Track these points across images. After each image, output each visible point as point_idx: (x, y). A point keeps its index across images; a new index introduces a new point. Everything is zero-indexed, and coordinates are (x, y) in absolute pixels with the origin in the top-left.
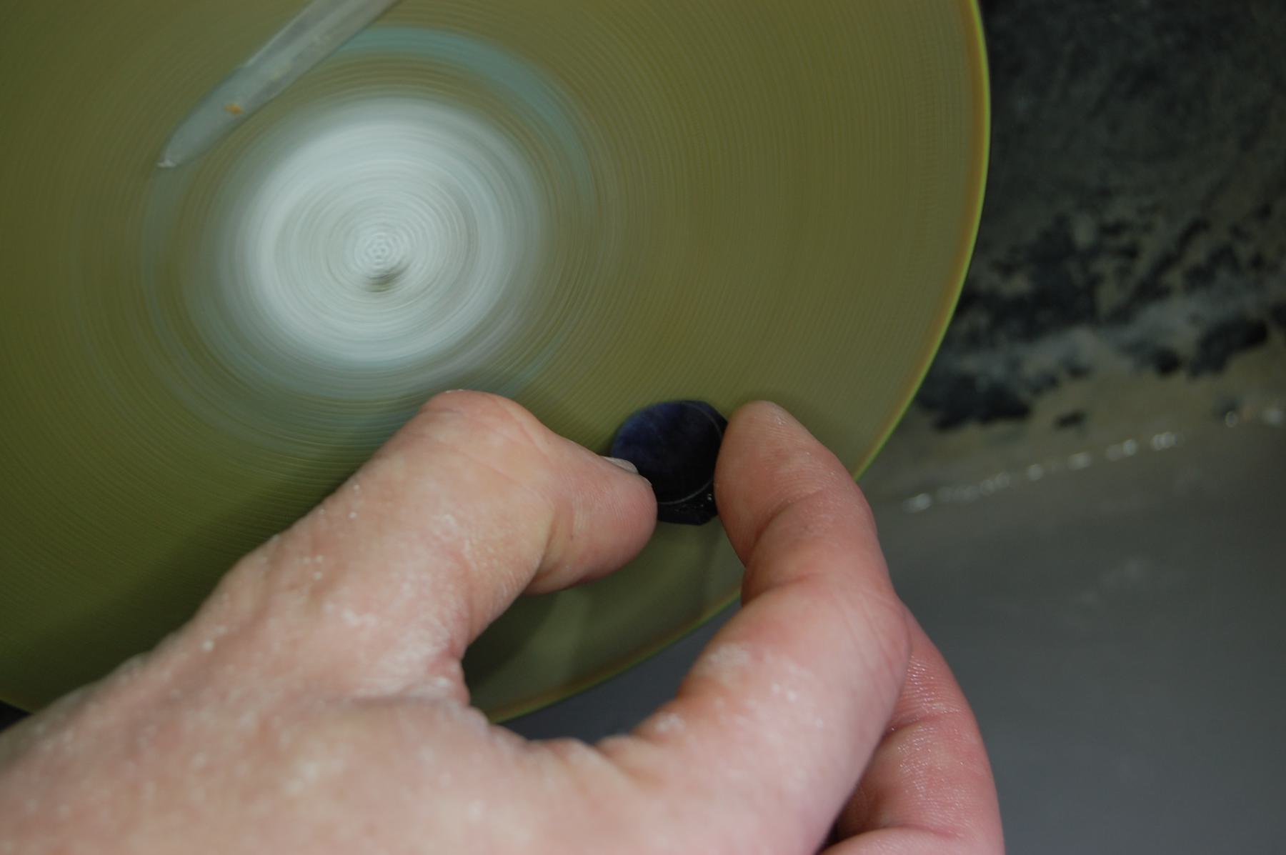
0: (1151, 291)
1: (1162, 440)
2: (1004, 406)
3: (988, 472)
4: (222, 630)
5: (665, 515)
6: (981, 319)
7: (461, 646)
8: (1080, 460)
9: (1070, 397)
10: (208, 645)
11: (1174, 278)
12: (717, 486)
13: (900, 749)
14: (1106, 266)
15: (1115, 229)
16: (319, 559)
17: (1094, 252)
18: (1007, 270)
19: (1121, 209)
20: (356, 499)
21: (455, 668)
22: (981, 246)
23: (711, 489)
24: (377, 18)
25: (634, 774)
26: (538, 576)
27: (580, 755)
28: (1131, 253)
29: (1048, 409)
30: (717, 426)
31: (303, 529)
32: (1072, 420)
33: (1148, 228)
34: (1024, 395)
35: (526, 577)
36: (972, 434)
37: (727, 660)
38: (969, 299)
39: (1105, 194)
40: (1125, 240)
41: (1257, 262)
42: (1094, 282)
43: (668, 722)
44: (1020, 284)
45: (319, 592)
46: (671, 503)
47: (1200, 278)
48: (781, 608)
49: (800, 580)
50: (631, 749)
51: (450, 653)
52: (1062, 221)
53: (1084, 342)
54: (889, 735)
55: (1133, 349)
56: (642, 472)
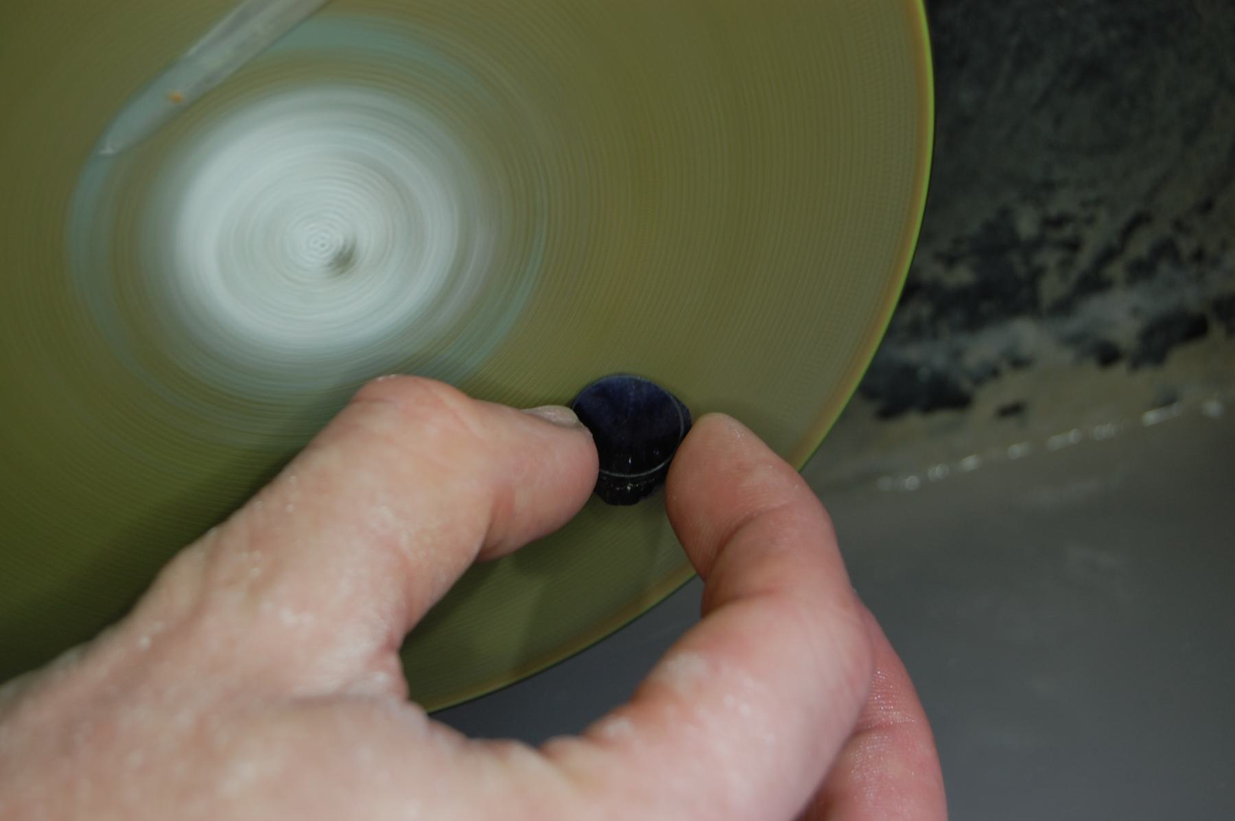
0: (1093, 284)
1: (1105, 430)
2: (946, 396)
3: (935, 462)
4: (158, 626)
6: (924, 310)
7: (398, 637)
8: (1017, 450)
9: (1011, 388)
10: (145, 642)
11: (1116, 270)
14: (1049, 258)
15: (1059, 222)
16: (257, 555)
17: (1037, 244)
18: (950, 261)
19: (1063, 202)
20: (293, 487)
21: (393, 661)
22: (926, 236)
24: (265, 471)
28: (1073, 246)
29: (989, 399)
30: (682, 427)
31: (241, 522)
32: (1013, 410)
33: (1090, 221)
34: (966, 385)
36: (914, 422)
37: (684, 669)
38: (912, 290)
39: (1049, 186)
40: (1068, 232)
41: (1199, 256)
42: (1036, 274)
43: (618, 727)
44: (963, 275)
45: (257, 590)
47: (1141, 270)
50: (577, 753)
51: (388, 647)
52: (1005, 213)
53: (1026, 334)
55: (1074, 341)
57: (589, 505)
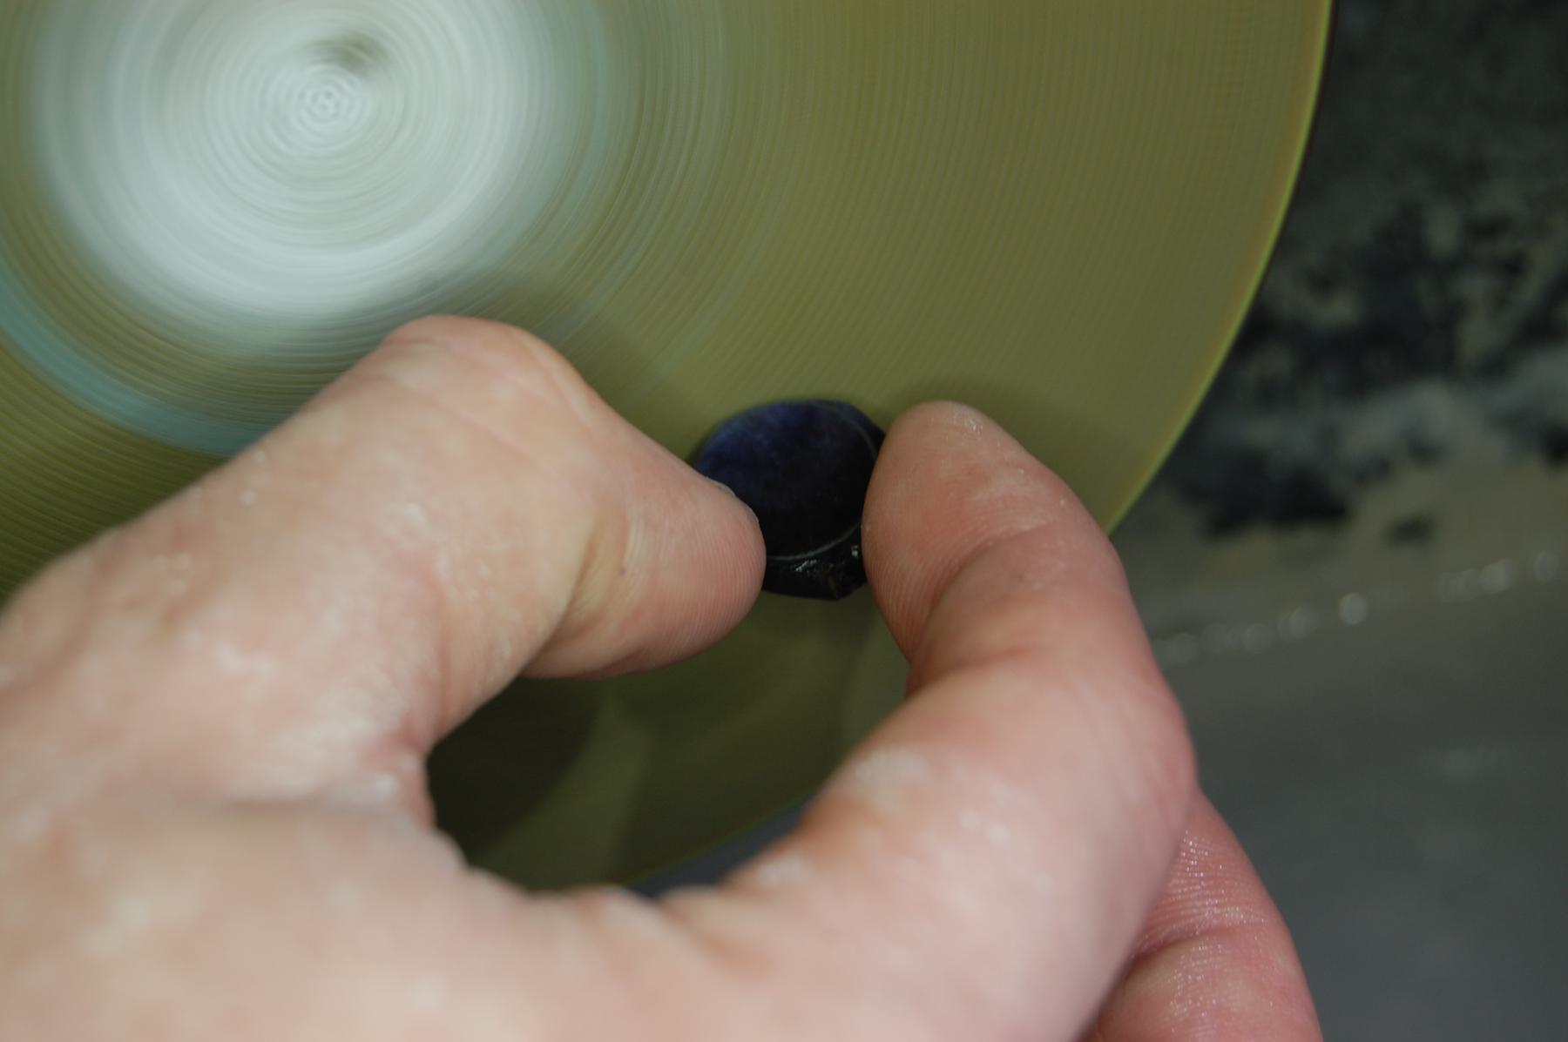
2: (1307, 502)
5: (776, 580)
6: (1276, 361)
7: (427, 735)
9: (1412, 492)
12: (867, 528)
13: (1166, 979)
14: (1475, 287)
15: (1491, 229)
16: (184, 561)
18: (1323, 284)
19: (1501, 198)
21: (411, 766)
22: (1286, 244)
23: (857, 538)
25: (722, 951)
26: (560, 636)
27: (624, 918)
28: (1514, 268)
29: (1375, 511)
30: (868, 441)
31: (161, 520)
32: (1413, 531)
35: (543, 627)
36: (1259, 547)
37: (884, 774)
38: (1259, 328)
40: (1505, 246)
42: (1454, 313)
43: (782, 871)
44: (1340, 310)
45: (174, 616)
46: (790, 558)
48: (983, 698)
49: (1013, 653)
50: (713, 911)
51: (404, 737)
53: (1436, 407)
54: (1139, 962)
55: (1514, 423)
56: (743, 495)
57: (756, 611)
